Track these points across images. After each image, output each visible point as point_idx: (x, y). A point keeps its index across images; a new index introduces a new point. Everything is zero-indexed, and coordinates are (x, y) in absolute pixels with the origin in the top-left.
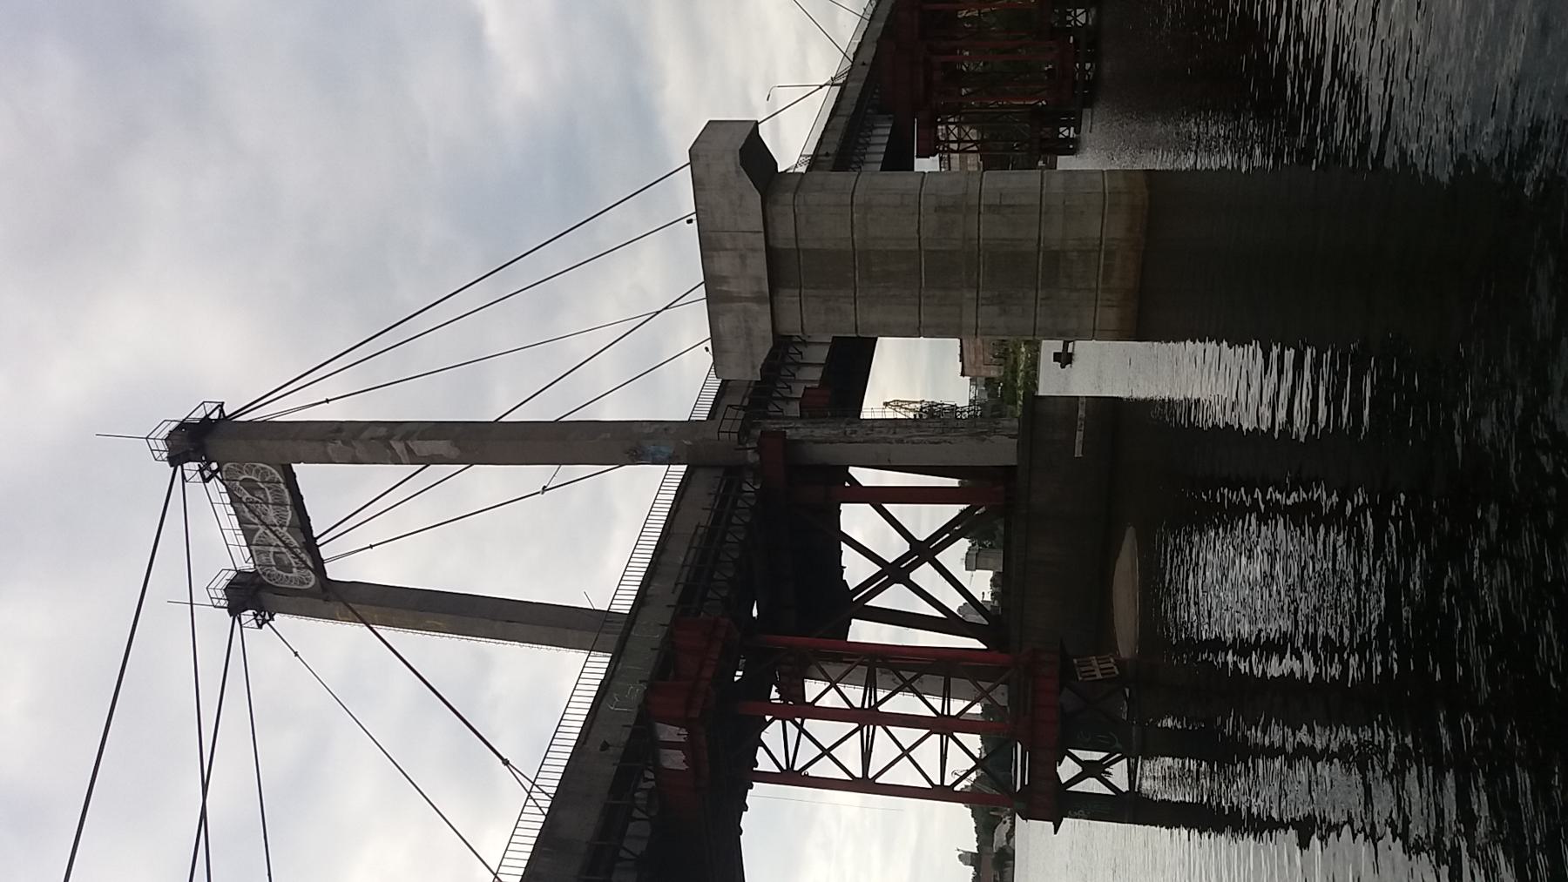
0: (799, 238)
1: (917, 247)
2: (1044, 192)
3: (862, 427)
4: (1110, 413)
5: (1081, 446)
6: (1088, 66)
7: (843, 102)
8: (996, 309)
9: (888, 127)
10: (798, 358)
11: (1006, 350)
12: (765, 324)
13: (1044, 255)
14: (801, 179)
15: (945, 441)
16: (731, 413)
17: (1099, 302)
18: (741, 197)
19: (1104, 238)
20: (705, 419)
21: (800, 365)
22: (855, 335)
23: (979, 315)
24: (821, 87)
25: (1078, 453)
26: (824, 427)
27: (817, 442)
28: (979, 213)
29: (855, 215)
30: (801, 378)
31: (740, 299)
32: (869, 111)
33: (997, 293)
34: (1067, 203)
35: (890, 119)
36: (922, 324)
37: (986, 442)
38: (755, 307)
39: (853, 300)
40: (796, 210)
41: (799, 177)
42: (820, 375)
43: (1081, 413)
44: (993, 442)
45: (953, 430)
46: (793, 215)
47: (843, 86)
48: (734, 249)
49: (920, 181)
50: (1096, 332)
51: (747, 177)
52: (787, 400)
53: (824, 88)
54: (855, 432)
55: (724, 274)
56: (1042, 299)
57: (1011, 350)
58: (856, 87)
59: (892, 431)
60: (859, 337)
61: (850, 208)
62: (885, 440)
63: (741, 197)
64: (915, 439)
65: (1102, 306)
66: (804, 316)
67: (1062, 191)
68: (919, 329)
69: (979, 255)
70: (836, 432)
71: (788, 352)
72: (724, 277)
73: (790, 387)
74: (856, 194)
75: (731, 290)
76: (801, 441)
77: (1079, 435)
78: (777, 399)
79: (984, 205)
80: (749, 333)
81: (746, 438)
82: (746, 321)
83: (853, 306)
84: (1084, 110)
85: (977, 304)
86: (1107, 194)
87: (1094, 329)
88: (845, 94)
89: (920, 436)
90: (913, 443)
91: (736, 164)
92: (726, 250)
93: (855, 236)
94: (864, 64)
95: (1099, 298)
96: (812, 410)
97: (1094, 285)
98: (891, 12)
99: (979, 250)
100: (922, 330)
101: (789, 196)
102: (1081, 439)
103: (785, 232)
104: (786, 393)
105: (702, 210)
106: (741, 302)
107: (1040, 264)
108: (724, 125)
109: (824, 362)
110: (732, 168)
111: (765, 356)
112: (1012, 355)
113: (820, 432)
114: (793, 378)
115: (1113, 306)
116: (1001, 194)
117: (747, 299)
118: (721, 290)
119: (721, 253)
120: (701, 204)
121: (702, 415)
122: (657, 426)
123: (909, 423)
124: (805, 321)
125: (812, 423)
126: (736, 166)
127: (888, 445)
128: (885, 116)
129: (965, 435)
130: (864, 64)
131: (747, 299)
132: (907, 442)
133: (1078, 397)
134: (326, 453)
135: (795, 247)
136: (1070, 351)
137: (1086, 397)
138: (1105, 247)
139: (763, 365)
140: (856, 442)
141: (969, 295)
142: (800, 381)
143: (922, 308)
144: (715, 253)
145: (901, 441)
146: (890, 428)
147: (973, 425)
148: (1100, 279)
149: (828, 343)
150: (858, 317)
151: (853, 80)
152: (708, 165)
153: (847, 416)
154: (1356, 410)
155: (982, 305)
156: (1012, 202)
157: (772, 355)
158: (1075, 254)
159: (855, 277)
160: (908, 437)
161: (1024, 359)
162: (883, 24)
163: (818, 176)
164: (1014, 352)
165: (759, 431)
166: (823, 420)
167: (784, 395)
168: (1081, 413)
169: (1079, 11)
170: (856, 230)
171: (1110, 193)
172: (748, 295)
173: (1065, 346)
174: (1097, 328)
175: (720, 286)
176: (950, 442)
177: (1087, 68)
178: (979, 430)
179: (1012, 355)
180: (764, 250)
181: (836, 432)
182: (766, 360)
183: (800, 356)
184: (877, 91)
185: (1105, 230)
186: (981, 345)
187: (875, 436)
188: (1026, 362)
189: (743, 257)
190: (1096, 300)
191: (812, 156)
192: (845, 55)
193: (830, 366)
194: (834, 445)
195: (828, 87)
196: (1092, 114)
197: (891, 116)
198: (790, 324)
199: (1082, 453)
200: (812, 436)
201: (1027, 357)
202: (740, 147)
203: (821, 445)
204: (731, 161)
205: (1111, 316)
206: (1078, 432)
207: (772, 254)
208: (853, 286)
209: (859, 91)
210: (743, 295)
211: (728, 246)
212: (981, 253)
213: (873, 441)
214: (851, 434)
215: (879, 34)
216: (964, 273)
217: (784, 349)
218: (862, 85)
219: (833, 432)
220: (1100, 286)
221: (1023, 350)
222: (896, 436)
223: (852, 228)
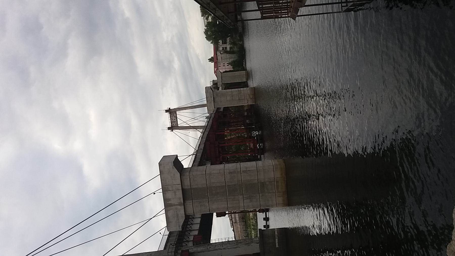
0: (191, 185)
1: (225, 184)
2: (257, 166)
3: (213, 246)
4: (284, 232)
5: (278, 243)
6: (261, 144)
7: (196, 159)
8: (248, 200)
9: (210, 164)
10: (190, 229)
11: (248, 233)
12: (182, 212)
13: (260, 184)
14: (191, 169)
15: (238, 247)
16: (171, 246)
17: (276, 196)
18: (174, 175)
19: (275, 177)
20: (163, 250)
21: (191, 231)
22: (209, 213)
23: (244, 203)
24: (190, 156)
25: (277, 246)
26: (201, 247)
27: (199, 252)
28: (241, 173)
29: (207, 177)
30: (192, 234)
31: (175, 205)
32: (204, 160)
33: (248, 196)
34: (264, 169)
35: (210, 162)
36: (229, 207)
37: (250, 246)
38: (179, 207)
39: (208, 202)
40: (190, 177)
41: (190, 169)
42: (197, 233)
43: (276, 233)
44: (252, 246)
45: (240, 243)
46: (189, 179)
47: (196, 155)
48: (173, 190)
49: (224, 166)
50: (277, 205)
51: (176, 169)
52: (188, 241)
53: (191, 156)
54: (210, 247)
55: (169, 198)
56: (261, 196)
57: (249, 233)
58: (199, 155)
59: (222, 246)
60: (210, 213)
61: (205, 175)
62: (220, 249)
63: (174, 175)
64: (229, 247)
65: (277, 197)
66: (194, 208)
67: (262, 166)
68: (228, 209)
69: (242, 185)
70: (205, 248)
71: (185, 234)
72: (169, 199)
73: (189, 238)
74: (206, 171)
75: (172, 202)
76: (194, 253)
77: (277, 240)
78: (185, 241)
79: (242, 171)
80: (177, 215)
81: (177, 254)
82: (176, 212)
83: (208, 204)
84: (262, 156)
85: (243, 199)
86: (274, 166)
87: (276, 204)
88: (197, 157)
89: (230, 246)
90: (228, 249)
91: (172, 165)
92: (170, 190)
93: (207, 183)
94: (201, 149)
95: (276, 194)
96: (196, 242)
97: (274, 191)
98: (207, 136)
99: (242, 184)
100: (228, 209)
101: (188, 173)
102: (277, 241)
103: (187, 183)
104: (188, 239)
105: (162, 180)
106: (175, 206)
107: (259, 186)
108: (168, 157)
109: (198, 229)
110: (171, 167)
111: (183, 222)
112: (250, 235)
113: (199, 249)
114: (189, 235)
115: (281, 197)
116: (246, 168)
117: (177, 205)
118: (169, 203)
119: (169, 192)
120: (162, 178)
121: (162, 248)
122: (148, 254)
123: (227, 243)
124: (194, 210)
125: (197, 246)
126: (172, 166)
127: (221, 250)
128: (209, 161)
129: (244, 244)
130: (201, 149)
131: (177, 205)
132: (227, 249)
133: (274, 229)
135: (190, 188)
136: (268, 224)
137: (277, 228)
138: (276, 180)
139: (182, 225)
140: (211, 251)
141: (241, 197)
142: (191, 235)
143: (228, 202)
144: (167, 192)
145: (225, 249)
146: (221, 245)
147: (246, 241)
148: (276, 189)
149: (199, 223)
150: (210, 207)
151: (199, 153)
152: (164, 167)
153: (208, 243)
154: (348, 231)
155: (245, 199)
156: (249, 170)
157: (185, 222)
158: (268, 183)
159: (208, 194)
160: (227, 247)
161: (254, 235)
162: (205, 139)
163: (196, 168)
164: (250, 234)
165: (181, 251)
166: (200, 245)
167: (187, 240)
168: (276, 233)
169: (257, 132)
170: (207, 181)
171: (274, 165)
172: (177, 204)
173: (267, 223)
174: (277, 203)
175: (168, 202)
176: (239, 247)
177: (261, 145)
178: (248, 242)
179: (250, 235)
180: (181, 189)
181: (205, 248)
182: (183, 224)
183: (191, 228)
184: (206, 155)
185: (275, 176)
186: (240, 234)
187: (217, 248)
188: (254, 236)
189: (175, 192)
190: (276, 195)
191: (168, 235)
192: (195, 149)
193: (201, 224)
194: (205, 252)
195: (191, 156)
196: (264, 157)
197: (210, 161)
198: (190, 211)
199: (278, 246)
200: (197, 250)
201: (254, 234)
202: (173, 161)
203: (200, 253)
204: (171, 165)
205: (280, 200)
206: (276, 239)
207: (183, 189)
208: (208, 197)
209: (201, 155)
210: (175, 204)
211: (171, 190)
212: (243, 184)
213: (216, 250)
214: (209, 248)
215: (204, 142)
216: (238, 191)
217: (188, 219)
218: (201, 154)
219: (204, 248)
220: (276, 191)
221: (253, 232)
222: (223, 247)
223: (206, 180)
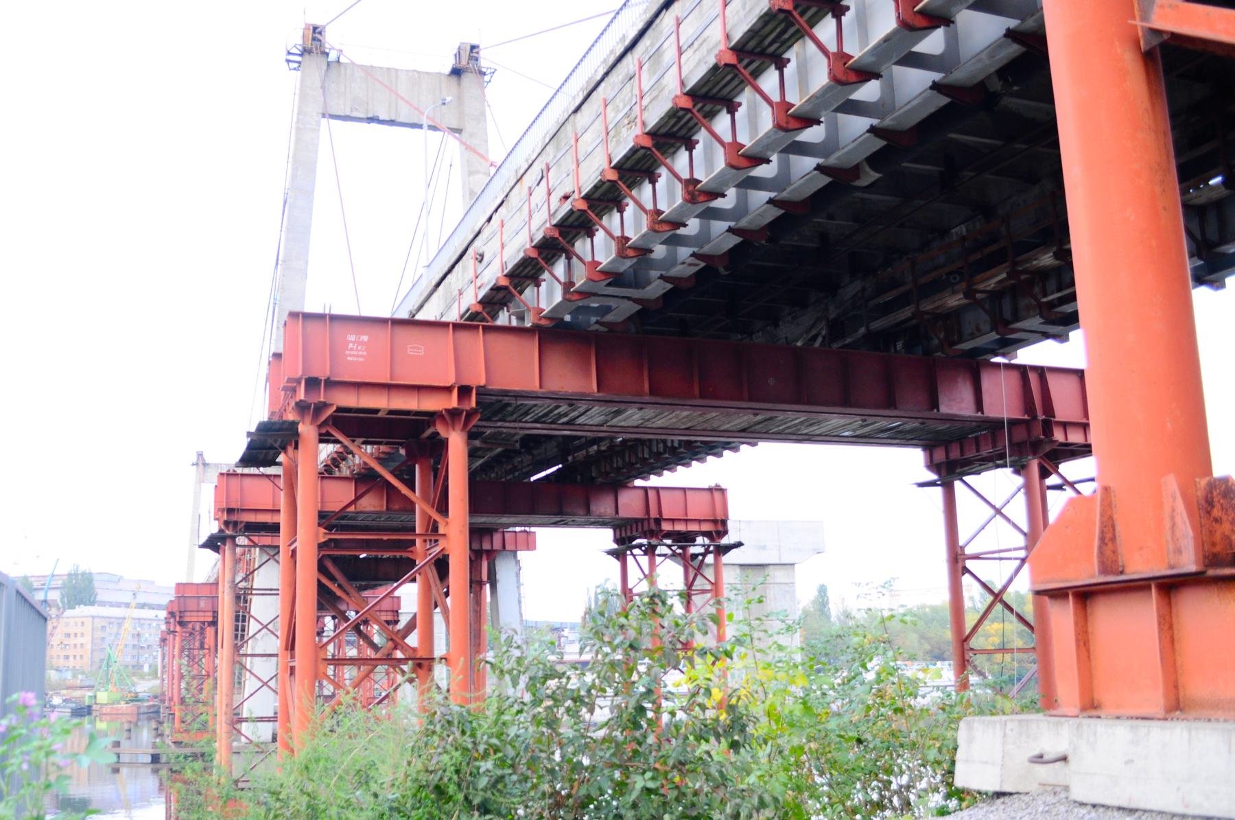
134: (478, 172)
